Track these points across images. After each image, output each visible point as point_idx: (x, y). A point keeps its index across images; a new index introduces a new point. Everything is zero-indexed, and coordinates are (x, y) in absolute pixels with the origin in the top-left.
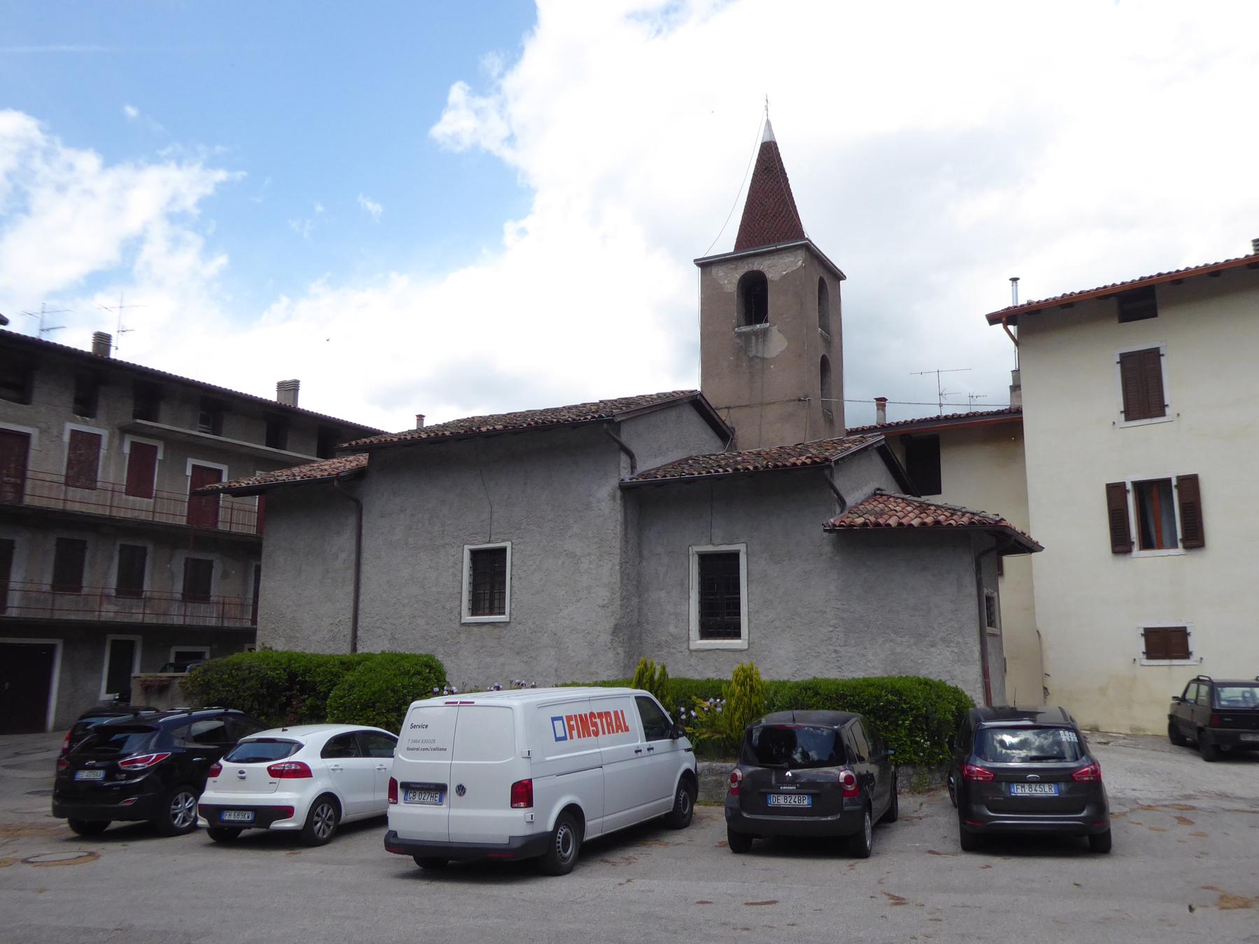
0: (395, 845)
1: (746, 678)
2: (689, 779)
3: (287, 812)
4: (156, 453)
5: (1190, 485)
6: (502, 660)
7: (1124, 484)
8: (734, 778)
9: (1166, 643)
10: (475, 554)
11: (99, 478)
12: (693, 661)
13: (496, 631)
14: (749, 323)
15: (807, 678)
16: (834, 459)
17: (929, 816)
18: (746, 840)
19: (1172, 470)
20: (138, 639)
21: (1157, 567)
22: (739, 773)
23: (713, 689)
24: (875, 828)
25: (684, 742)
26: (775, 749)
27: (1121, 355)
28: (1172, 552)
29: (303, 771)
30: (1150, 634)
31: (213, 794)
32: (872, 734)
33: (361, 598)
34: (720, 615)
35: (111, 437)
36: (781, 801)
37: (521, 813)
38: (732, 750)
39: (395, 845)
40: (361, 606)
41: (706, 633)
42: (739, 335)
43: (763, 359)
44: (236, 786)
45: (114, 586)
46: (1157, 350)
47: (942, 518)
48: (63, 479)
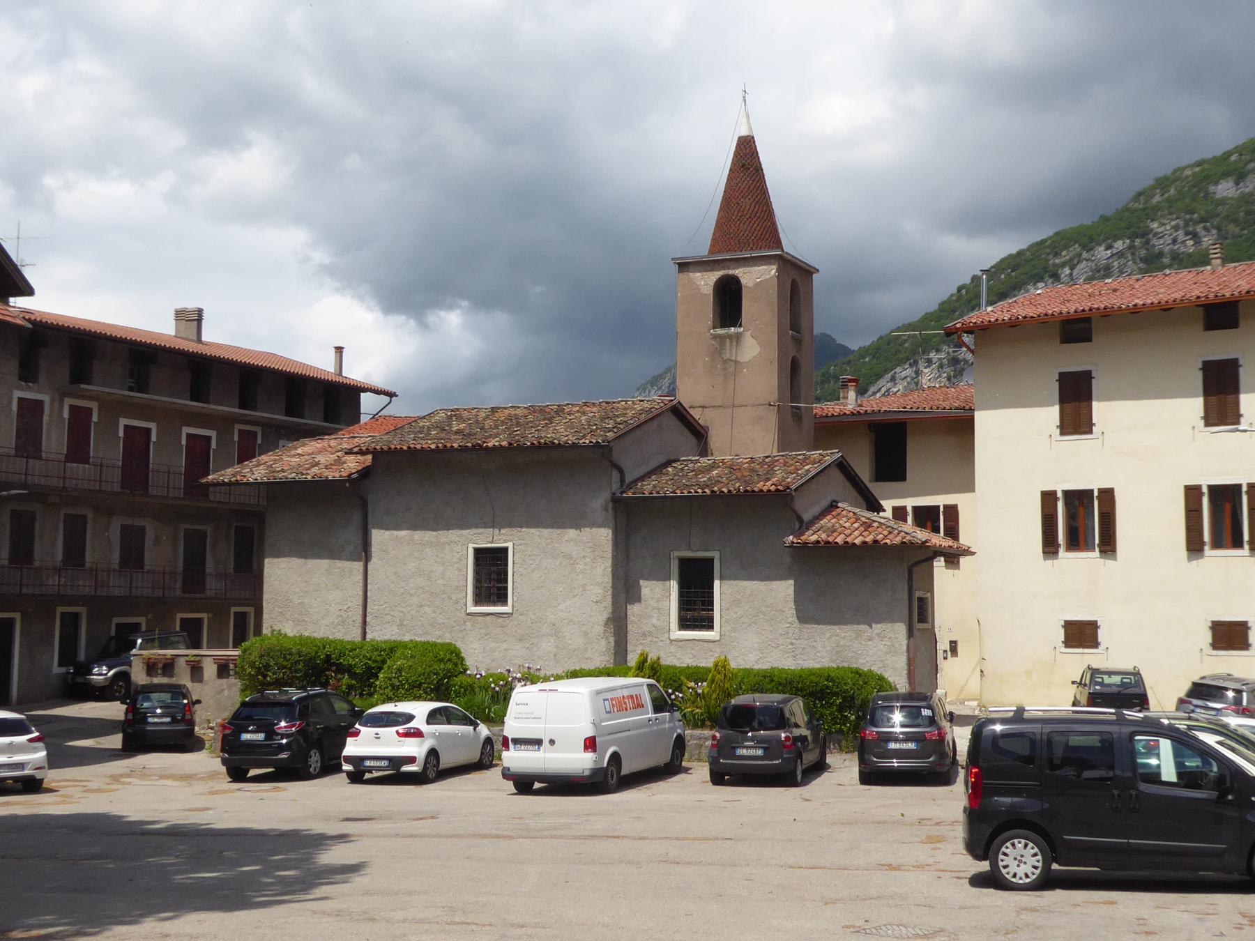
0: (507, 774)
1: (721, 666)
2: (680, 743)
3: (412, 760)
4: (91, 414)
5: (1107, 496)
6: (505, 645)
7: (1055, 492)
8: (714, 737)
9: (1081, 634)
10: (478, 551)
11: (44, 449)
12: (673, 649)
13: (500, 620)
14: (723, 326)
15: (765, 667)
16: (793, 487)
17: (844, 767)
18: (718, 778)
19: (1093, 483)
20: (82, 610)
21: (1078, 565)
22: (718, 735)
23: (697, 674)
24: (804, 772)
25: (677, 715)
26: (739, 720)
27: (1060, 374)
28: (1090, 554)
29: (417, 734)
30: (1069, 625)
31: (352, 748)
32: (809, 711)
33: (369, 587)
34: (696, 611)
35: (52, 401)
36: (744, 752)
37: (590, 756)
38: (708, 723)
39: (507, 774)
40: (369, 594)
41: (684, 624)
42: (715, 337)
43: (736, 362)
44: (365, 743)
45: (60, 559)
46: (1090, 372)
47: (880, 537)
48: (13, 452)
